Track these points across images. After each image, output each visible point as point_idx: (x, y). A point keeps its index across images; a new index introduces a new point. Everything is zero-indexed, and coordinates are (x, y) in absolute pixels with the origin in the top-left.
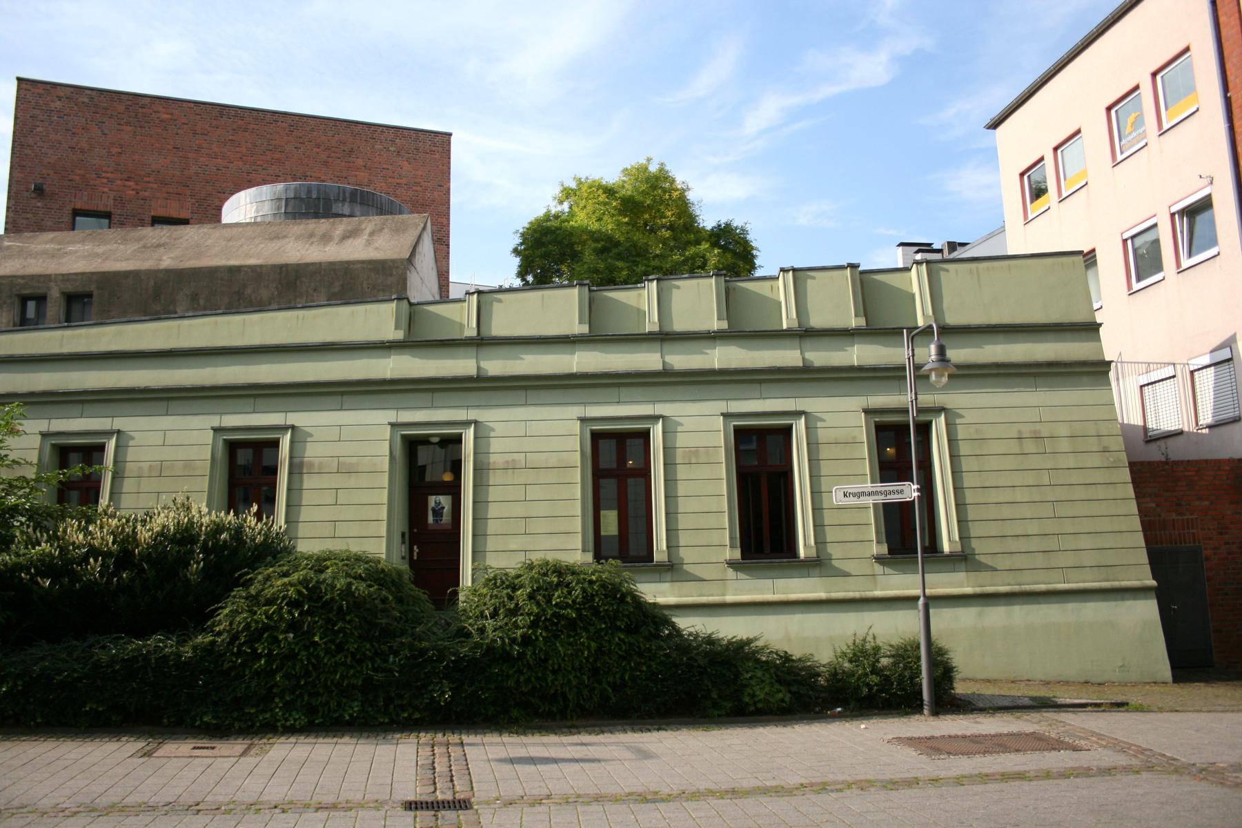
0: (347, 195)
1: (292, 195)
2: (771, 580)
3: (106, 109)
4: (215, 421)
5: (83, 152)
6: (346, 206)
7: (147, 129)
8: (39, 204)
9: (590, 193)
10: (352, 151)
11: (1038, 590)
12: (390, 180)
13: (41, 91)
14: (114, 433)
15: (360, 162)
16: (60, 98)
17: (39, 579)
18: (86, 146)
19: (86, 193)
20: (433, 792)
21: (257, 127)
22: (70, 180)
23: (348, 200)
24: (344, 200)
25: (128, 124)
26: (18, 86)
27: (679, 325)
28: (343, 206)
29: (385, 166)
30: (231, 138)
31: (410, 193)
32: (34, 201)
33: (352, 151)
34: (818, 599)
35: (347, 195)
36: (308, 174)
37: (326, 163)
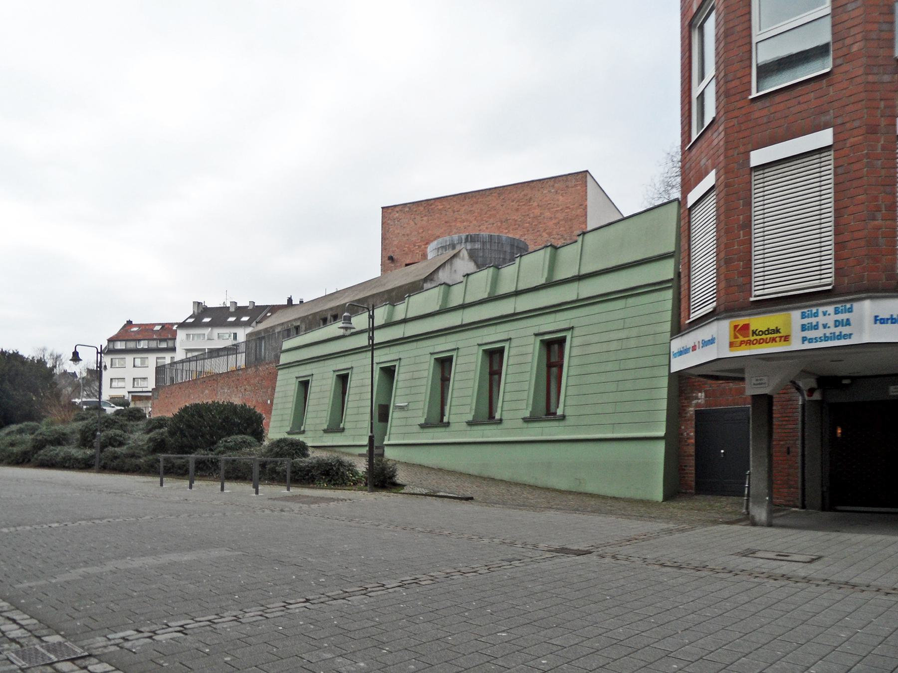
3: (416, 211)
5: (408, 235)
8: (393, 265)
9: (568, 208)
10: (531, 198)
15: (535, 204)
16: (397, 212)
17: (710, 180)
18: (408, 232)
23: (463, 242)
25: (425, 216)
27: (452, 407)
29: (549, 202)
31: (564, 214)
32: (390, 264)
33: (531, 198)
37: (517, 210)
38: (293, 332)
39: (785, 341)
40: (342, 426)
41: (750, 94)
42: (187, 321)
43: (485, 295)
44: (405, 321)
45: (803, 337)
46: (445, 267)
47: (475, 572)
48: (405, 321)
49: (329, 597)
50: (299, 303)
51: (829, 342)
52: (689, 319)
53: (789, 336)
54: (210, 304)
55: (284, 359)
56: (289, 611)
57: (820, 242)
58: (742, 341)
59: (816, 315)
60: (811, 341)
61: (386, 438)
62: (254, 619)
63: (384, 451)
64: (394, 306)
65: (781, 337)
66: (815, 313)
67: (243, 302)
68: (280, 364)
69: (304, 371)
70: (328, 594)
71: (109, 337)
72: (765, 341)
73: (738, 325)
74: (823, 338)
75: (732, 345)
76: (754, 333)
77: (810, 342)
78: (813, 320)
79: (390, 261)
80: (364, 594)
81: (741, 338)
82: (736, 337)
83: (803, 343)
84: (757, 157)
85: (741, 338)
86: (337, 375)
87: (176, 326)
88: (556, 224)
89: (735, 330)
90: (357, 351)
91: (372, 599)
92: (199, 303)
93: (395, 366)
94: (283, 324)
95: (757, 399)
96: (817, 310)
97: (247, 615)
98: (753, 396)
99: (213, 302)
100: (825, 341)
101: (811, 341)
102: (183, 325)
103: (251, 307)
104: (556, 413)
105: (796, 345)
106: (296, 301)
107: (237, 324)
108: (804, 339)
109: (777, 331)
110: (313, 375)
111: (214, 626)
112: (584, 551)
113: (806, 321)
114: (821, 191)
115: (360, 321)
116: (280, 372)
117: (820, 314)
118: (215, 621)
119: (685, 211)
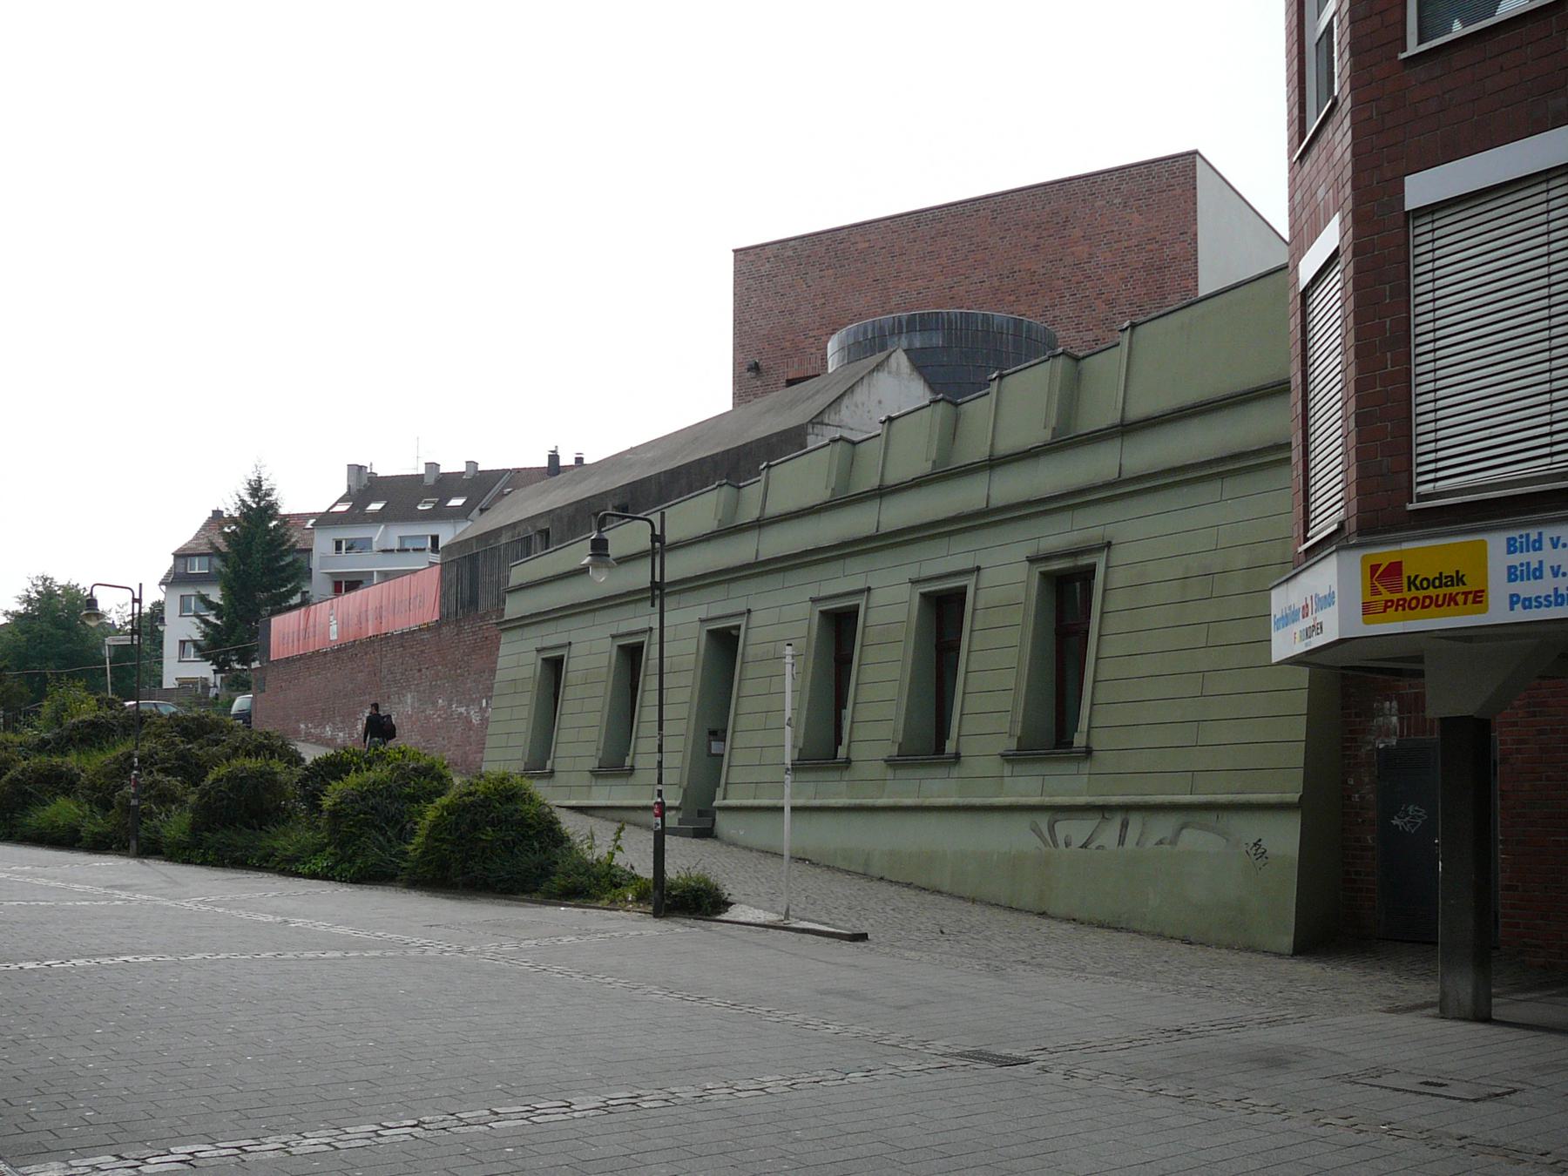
0: (904, 324)
1: (851, 341)
2: (1302, 766)
4: (913, 572)
6: (903, 339)
7: (847, 267)
8: (759, 383)
11: (1153, 803)
12: (1115, 246)
13: (752, 258)
14: (864, 592)
15: (1078, 232)
19: (796, 359)
20: (1056, 822)
21: (956, 226)
22: (782, 349)
23: (905, 330)
24: (900, 333)
26: (735, 256)
28: (899, 339)
30: (930, 249)
34: (945, 805)
35: (904, 324)
36: (1016, 268)
38: (537, 541)
39: (1475, 602)
40: (628, 761)
41: (1405, 50)
42: (335, 509)
43: (925, 468)
44: (760, 524)
45: (1512, 596)
46: (852, 392)
47: (761, 1089)
48: (760, 524)
49: (460, 1119)
50: (573, 463)
51: (1553, 608)
52: (1306, 540)
53: (1483, 591)
54: (383, 470)
55: (515, 607)
56: (380, 1140)
57: (1551, 381)
58: (1387, 601)
59: (1537, 546)
60: (1527, 604)
61: (719, 792)
62: (318, 1148)
63: (714, 820)
64: (740, 488)
65: (1466, 594)
66: (1535, 541)
67: (452, 464)
68: (506, 618)
69: (551, 636)
70: (461, 1115)
71: (175, 548)
72: (1435, 602)
73: (1380, 565)
74: (1552, 599)
75: (1367, 609)
76: (1411, 583)
77: (1525, 608)
78: (1533, 558)
79: (753, 374)
80: (527, 1119)
81: (1386, 595)
82: (1375, 592)
83: (1512, 609)
84: (1421, 189)
85: (1386, 595)
86: (620, 647)
87: (312, 521)
88: (1125, 280)
89: (1372, 575)
90: (618, 601)
91: (535, 1129)
92: (361, 468)
93: (738, 627)
94: (514, 526)
95: (1450, 725)
96: (1540, 534)
97: (306, 1142)
98: (1441, 718)
99: (392, 463)
100: (1547, 606)
101: (1527, 604)
102: (326, 520)
103: (472, 473)
104: (1072, 743)
105: (1497, 612)
106: (566, 460)
107: (440, 514)
108: (1514, 600)
109: (1459, 579)
110: (570, 643)
111: (243, 1156)
112: (1015, 1059)
113: (1517, 559)
114: (1549, 265)
115: (628, 537)
116: (504, 638)
117: (1547, 544)
118: (248, 1149)
119: (1295, 297)
